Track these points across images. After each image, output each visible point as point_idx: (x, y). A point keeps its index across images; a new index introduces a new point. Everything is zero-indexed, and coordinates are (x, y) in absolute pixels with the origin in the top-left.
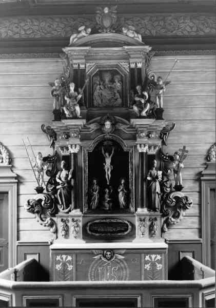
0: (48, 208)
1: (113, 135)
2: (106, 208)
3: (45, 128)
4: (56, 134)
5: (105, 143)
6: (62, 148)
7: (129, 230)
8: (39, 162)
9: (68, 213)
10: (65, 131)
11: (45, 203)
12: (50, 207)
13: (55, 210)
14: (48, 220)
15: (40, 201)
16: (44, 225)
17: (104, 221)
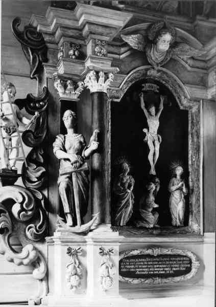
0: (27, 223)
1: (164, 69)
2: (148, 222)
3: (21, 28)
4: (46, 48)
5: (146, 87)
6: (63, 79)
7: (194, 270)
8: (8, 109)
9: (84, 233)
10: (74, 40)
11: (22, 209)
12: (33, 219)
13: (44, 227)
14: (28, 250)
15: (9, 203)
16: (17, 261)
17: (149, 252)
